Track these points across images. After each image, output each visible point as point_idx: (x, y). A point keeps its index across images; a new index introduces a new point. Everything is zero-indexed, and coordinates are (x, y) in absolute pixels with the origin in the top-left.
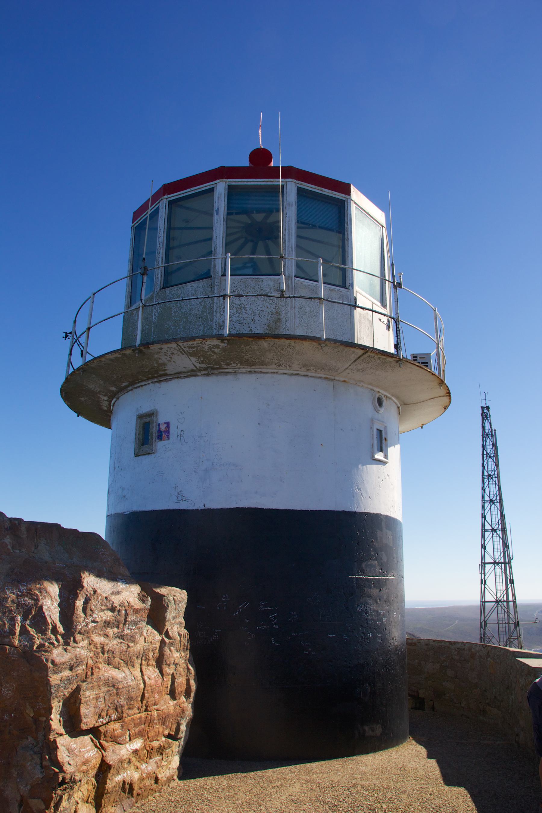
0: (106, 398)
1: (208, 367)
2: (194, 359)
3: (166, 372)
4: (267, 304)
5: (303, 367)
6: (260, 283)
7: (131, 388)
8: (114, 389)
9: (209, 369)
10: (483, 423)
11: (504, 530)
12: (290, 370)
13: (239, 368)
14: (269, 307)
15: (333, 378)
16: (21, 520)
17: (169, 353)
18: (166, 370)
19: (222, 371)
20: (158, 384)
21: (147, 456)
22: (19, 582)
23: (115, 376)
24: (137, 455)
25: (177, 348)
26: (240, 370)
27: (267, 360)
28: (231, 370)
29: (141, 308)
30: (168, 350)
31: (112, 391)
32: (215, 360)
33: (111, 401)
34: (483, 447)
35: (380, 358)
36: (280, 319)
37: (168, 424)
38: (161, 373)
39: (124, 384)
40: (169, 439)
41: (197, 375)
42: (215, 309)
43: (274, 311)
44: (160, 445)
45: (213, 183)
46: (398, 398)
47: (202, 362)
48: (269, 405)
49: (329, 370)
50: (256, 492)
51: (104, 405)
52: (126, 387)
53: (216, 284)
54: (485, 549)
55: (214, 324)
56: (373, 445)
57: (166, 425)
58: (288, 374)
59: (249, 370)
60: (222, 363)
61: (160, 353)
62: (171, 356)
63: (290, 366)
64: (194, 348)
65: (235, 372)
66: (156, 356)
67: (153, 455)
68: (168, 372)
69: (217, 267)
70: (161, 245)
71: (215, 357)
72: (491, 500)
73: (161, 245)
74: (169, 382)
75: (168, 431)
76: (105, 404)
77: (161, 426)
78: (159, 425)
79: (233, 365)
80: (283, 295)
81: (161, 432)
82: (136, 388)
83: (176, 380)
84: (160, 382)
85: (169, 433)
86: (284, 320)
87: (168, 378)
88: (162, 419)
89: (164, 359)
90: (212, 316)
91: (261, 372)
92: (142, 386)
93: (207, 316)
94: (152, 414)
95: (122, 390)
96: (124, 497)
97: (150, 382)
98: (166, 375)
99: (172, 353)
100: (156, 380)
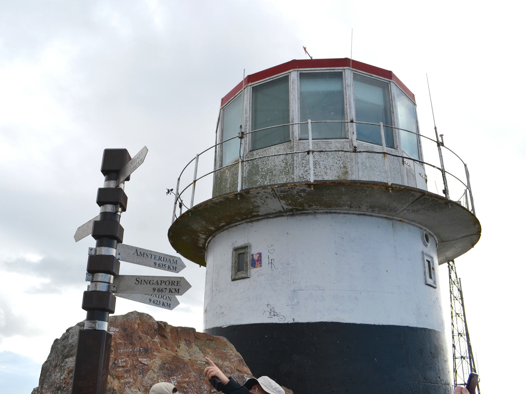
0: (204, 237)
1: (293, 209)
2: (283, 202)
3: (259, 213)
4: (336, 161)
5: (370, 208)
6: (330, 145)
7: (226, 227)
8: (213, 228)
9: (294, 211)
10: (450, 273)
11: (471, 358)
12: (359, 211)
13: (318, 210)
14: (338, 162)
15: (392, 217)
16: (165, 324)
17: (264, 197)
18: (259, 211)
19: (304, 212)
20: (250, 224)
21: (242, 280)
22: (170, 376)
23: (216, 217)
24: (234, 280)
25: (271, 193)
26: (319, 211)
27: (342, 202)
28: (311, 211)
29: (240, 163)
30: (264, 194)
31: (211, 230)
32: (300, 202)
33: (207, 239)
34: (451, 292)
35: (433, 200)
36: (347, 172)
37: (260, 254)
38: (254, 214)
39: (222, 224)
40: (261, 266)
41: (283, 216)
42: (295, 165)
43: (342, 166)
44: (253, 272)
45: (288, 72)
46: (438, 236)
47: (290, 205)
48: (343, 238)
49: (390, 211)
50: (337, 309)
51: (201, 242)
52: (223, 226)
53: (295, 146)
54: (456, 372)
55: (295, 176)
56: (425, 272)
57: (258, 255)
58: (357, 214)
59: (326, 211)
60: (305, 205)
61: (256, 197)
62: (265, 199)
63: (359, 207)
64: (285, 192)
65: (315, 213)
66: (253, 200)
67: (248, 280)
68: (260, 213)
69: (295, 134)
70: (248, 119)
71: (300, 200)
72: (459, 334)
73: (248, 119)
74: (260, 222)
75: (260, 260)
76: (202, 241)
77: (254, 256)
78: (253, 255)
79: (314, 207)
80: (355, 150)
81: (255, 260)
82: (231, 227)
83: (266, 220)
84: (251, 222)
85: (261, 261)
86: (350, 172)
87: (259, 218)
88: (254, 251)
89: (259, 202)
90: (293, 170)
91: (335, 213)
92: (236, 225)
93: (289, 170)
94: (245, 247)
95: (219, 229)
96: (223, 313)
97: (244, 222)
98: (258, 216)
99: (267, 197)
100: (248, 220)
